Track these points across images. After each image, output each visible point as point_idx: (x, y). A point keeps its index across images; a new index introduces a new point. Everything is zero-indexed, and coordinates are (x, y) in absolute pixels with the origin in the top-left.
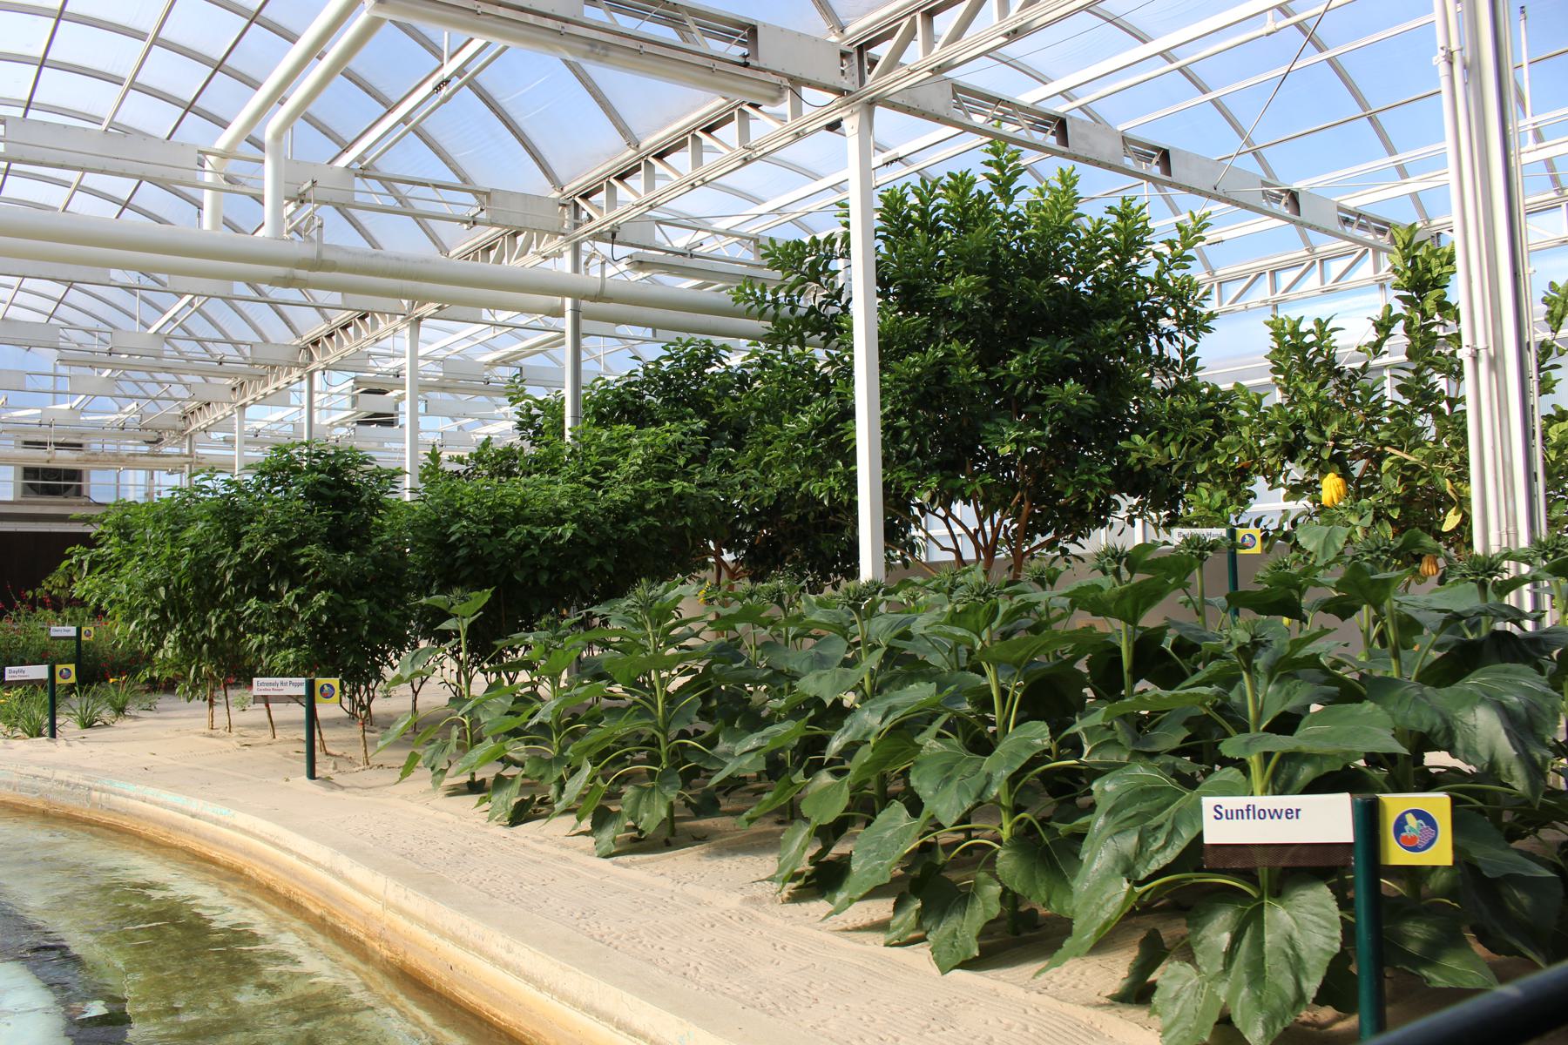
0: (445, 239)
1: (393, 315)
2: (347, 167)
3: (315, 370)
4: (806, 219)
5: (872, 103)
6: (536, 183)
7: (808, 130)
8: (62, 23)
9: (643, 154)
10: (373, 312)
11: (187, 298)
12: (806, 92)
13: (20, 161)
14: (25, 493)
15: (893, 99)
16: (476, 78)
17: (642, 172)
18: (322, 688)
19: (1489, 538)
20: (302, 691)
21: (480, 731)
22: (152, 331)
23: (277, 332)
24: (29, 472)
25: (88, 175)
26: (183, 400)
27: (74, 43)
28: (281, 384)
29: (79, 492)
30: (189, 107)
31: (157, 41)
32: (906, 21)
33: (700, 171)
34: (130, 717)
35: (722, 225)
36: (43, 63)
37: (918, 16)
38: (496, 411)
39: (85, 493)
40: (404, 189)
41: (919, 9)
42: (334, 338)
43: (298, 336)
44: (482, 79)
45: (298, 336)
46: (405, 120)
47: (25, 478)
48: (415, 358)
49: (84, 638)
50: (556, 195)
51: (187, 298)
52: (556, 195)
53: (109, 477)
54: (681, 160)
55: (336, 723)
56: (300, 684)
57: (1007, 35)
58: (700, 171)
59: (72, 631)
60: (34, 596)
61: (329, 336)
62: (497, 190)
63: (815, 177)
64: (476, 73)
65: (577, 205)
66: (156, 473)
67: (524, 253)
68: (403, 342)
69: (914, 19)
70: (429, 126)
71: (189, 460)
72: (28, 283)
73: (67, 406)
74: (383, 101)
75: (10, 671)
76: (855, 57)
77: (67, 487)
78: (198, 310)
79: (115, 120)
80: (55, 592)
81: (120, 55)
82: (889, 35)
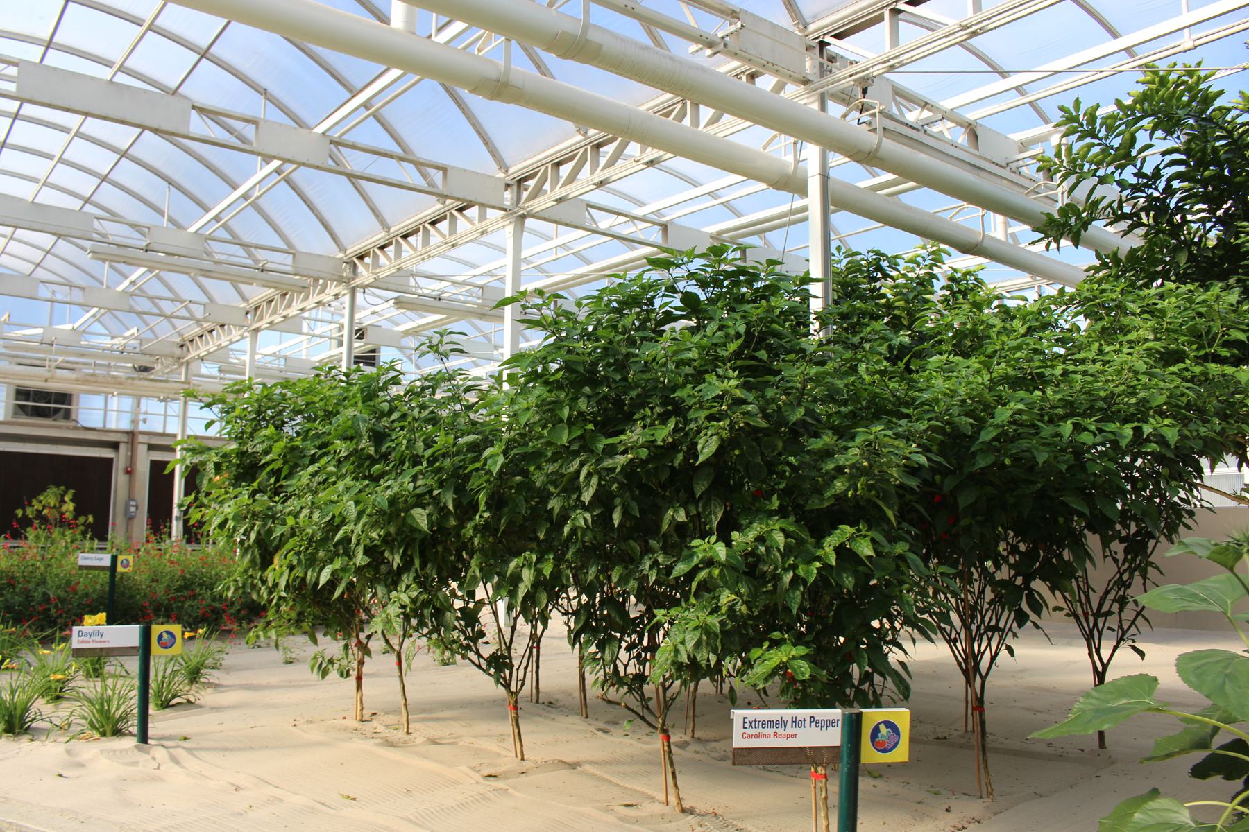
0: (247, 295)
2: (324, 133)
3: (357, 286)
5: (523, 217)
6: (489, 167)
8: (50, 50)
11: (275, 164)
12: (489, 211)
13: (30, 102)
14: (15, 414)
15: (541, 214)
16: (381, 111)
17: (420, 234)
18: (876, 730)
20: (833, 737)
23: (317, 242)
24: (22, 393)
25: (18, 230)
28: (293, 311)
29: (67, 415)
30: (204, 54)
31: (46, 184)
32: (582, 150)
34: (210, 685)
37: (589, 147)
38: (495, 353)
39: (73, 417)
41: (887, 6)
42: (214, 333)
43: (342, 249)
44: (385, 113)
45: (342, 249)
46: (366, 105)
47: (17, 399)
48: (253, 353)
49: (120, 569)
50: (341, 255)
51: (275, 164)
53: (98, 401)
55: (683, 745)
56: (833, 723)
57: (556, 200)
59: (106, 560)
62: (747, 12)
64: (381, 107)
65: (355, 264)
66: (143, 401)
68: (246, 344)
69: (586, 149)
70: (264, 203)
72: (20, 233)
74: (351, 91)
75: (80, 634)
76: (515, 188)
77: (57, 410)
78: (288, 181)
79: (81, 130)
80: (45, 512)
82: (571, 159)
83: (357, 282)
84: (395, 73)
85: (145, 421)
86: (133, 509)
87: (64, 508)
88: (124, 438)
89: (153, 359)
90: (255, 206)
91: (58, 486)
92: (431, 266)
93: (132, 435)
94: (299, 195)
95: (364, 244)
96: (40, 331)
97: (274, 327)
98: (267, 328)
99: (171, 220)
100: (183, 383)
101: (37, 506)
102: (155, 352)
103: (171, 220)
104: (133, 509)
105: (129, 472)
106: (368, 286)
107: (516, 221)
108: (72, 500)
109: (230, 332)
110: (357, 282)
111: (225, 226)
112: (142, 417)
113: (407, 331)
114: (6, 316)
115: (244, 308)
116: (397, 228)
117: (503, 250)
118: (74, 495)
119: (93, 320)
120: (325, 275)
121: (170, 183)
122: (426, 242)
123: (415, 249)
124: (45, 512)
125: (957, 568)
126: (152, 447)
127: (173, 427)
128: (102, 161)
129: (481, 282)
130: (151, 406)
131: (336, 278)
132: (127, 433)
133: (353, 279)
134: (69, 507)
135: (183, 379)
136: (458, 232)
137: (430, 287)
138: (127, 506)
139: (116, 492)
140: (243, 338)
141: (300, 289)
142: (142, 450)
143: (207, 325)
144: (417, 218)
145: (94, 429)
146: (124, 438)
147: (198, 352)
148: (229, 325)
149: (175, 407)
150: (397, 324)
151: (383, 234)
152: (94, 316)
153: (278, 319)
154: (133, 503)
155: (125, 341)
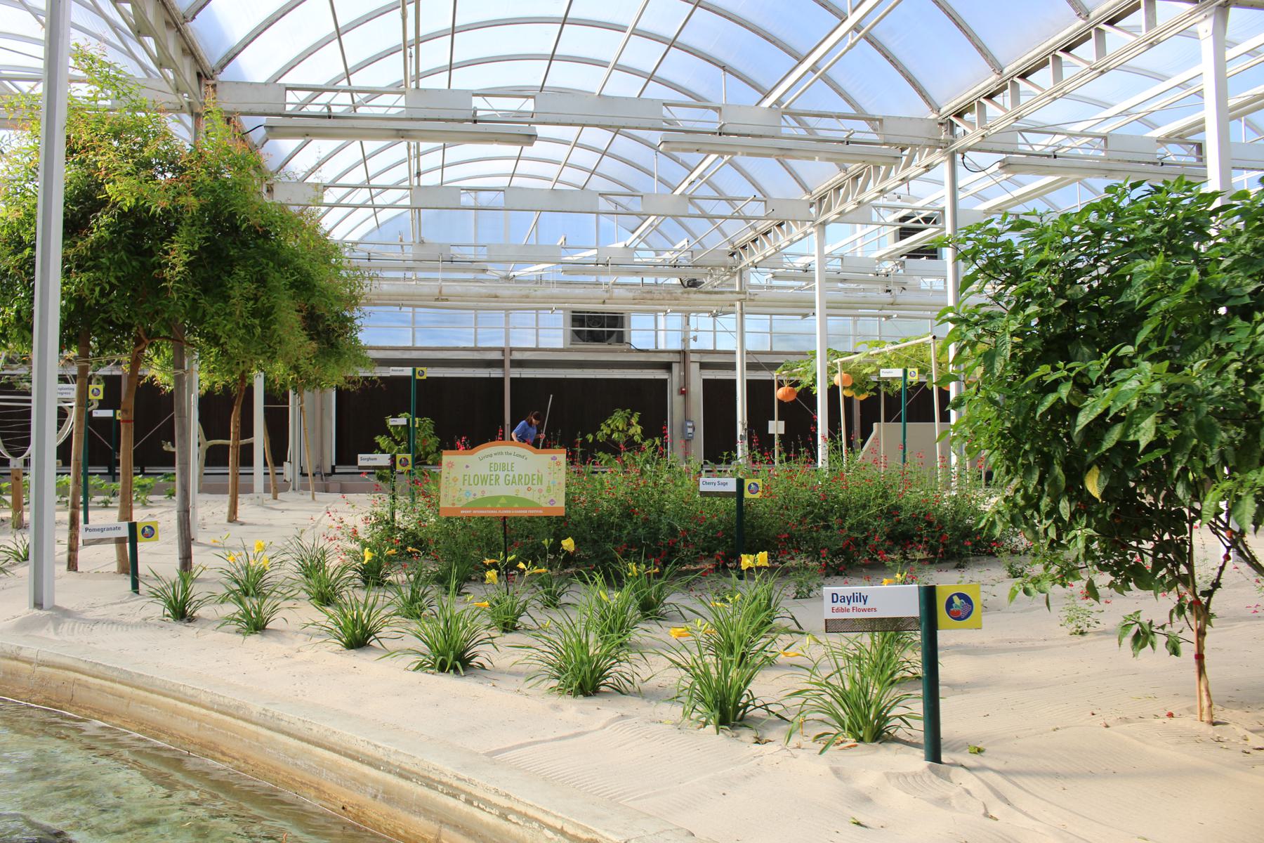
1: (804, 221)
2: (770, 107)
4: (1149, 117)
6: (920, 109)
7: (1162, 39)
9: (1092, 24)
10: (788, 220)
14: (573, 341)
16: (871, 32)
17: (1008, 91)
19: (1019, 480)
21: (577, 583)
22: (678, 192)
26: (759, 219)
27: (576, 40)
29: (620, 338)
33: (1153, 32)
35: (1077, 128)
36: (552, 58)
39: (626, 340)
40: (811, 121)
42: (758, 242)
43: (807, 190)
45: (807, 190)
46: (814, 69)
48: (823, 257)
50: (934, 116)
52: (934, 116)
54: (1044, 77)
58: (1153, 32)
60: (595, 439)
61: (754, 241)
63: (1161, 78)
64: (790, 103)
65: (952, 122)
66: (693, 319)
67: (908, 164)
71: (742, 296)
73: (621, 245)
74: (797, 58)
77: (610, 334)
81: (604, 45)
83: (958, 145)
84: (713, 157)
85: (695, 339)
86: (690, 430)
87: (632, 431)
88: (676, 358)
89: (704, 270)
90: (825, 78)
91: (623, 409)
92: (1048, 115)
93: (683, 353)
94: (879, 50)
95: (966, 96)
96: (594, 252)
97: (843, 219)
98: (834, 221)
99: (660, 180)
100: (738, 293)
101: (606, 430)
102: (707, 264)
103: (660, 180)
104: (690, 430)
105: (684, 393)
106: (969, 149)
107: (1215, 13)
108: (638, 423)
109: (790, 231)
110: (958, 145)
111: (708, 182)
112: (692, 334)
113: (989, 209)
114: (562, 240)
115: (808, 200)
116: (1014, 66)
117: (941, 183)
118: (640, 417)
119: (638, 240)
120: (917, 141)
121: (723, 68)
122: (1058, 75)
123: (1002, 108)
124: (615, 436)
125: (643, 440)
126: (703, 366)
127: (727, 343)
128: (590, 159)
129: (1103, 130)
130: (701, 322)
131: (931, 142)
132: (679, 352)
133: (952, 142)
134: (636, 430)
135: (737, 289)
136: (1064, 79)
137: (1042, 143)
138: (684, 428)
139: (672, 413)
140: (806, 235)
141: (891, 160)
142: (694, 368)
143: (762, 226)
144: (1043, 47)
145: (647, 351)
146: (676, 358)
147: (752, 259)
148: (788, 220)
149: (729, 322)
150: (1154, 126)
151: (994, 77)
152: (651, 225)
153: (850, 206)
154: (689, 424)
155: (675, 256)
